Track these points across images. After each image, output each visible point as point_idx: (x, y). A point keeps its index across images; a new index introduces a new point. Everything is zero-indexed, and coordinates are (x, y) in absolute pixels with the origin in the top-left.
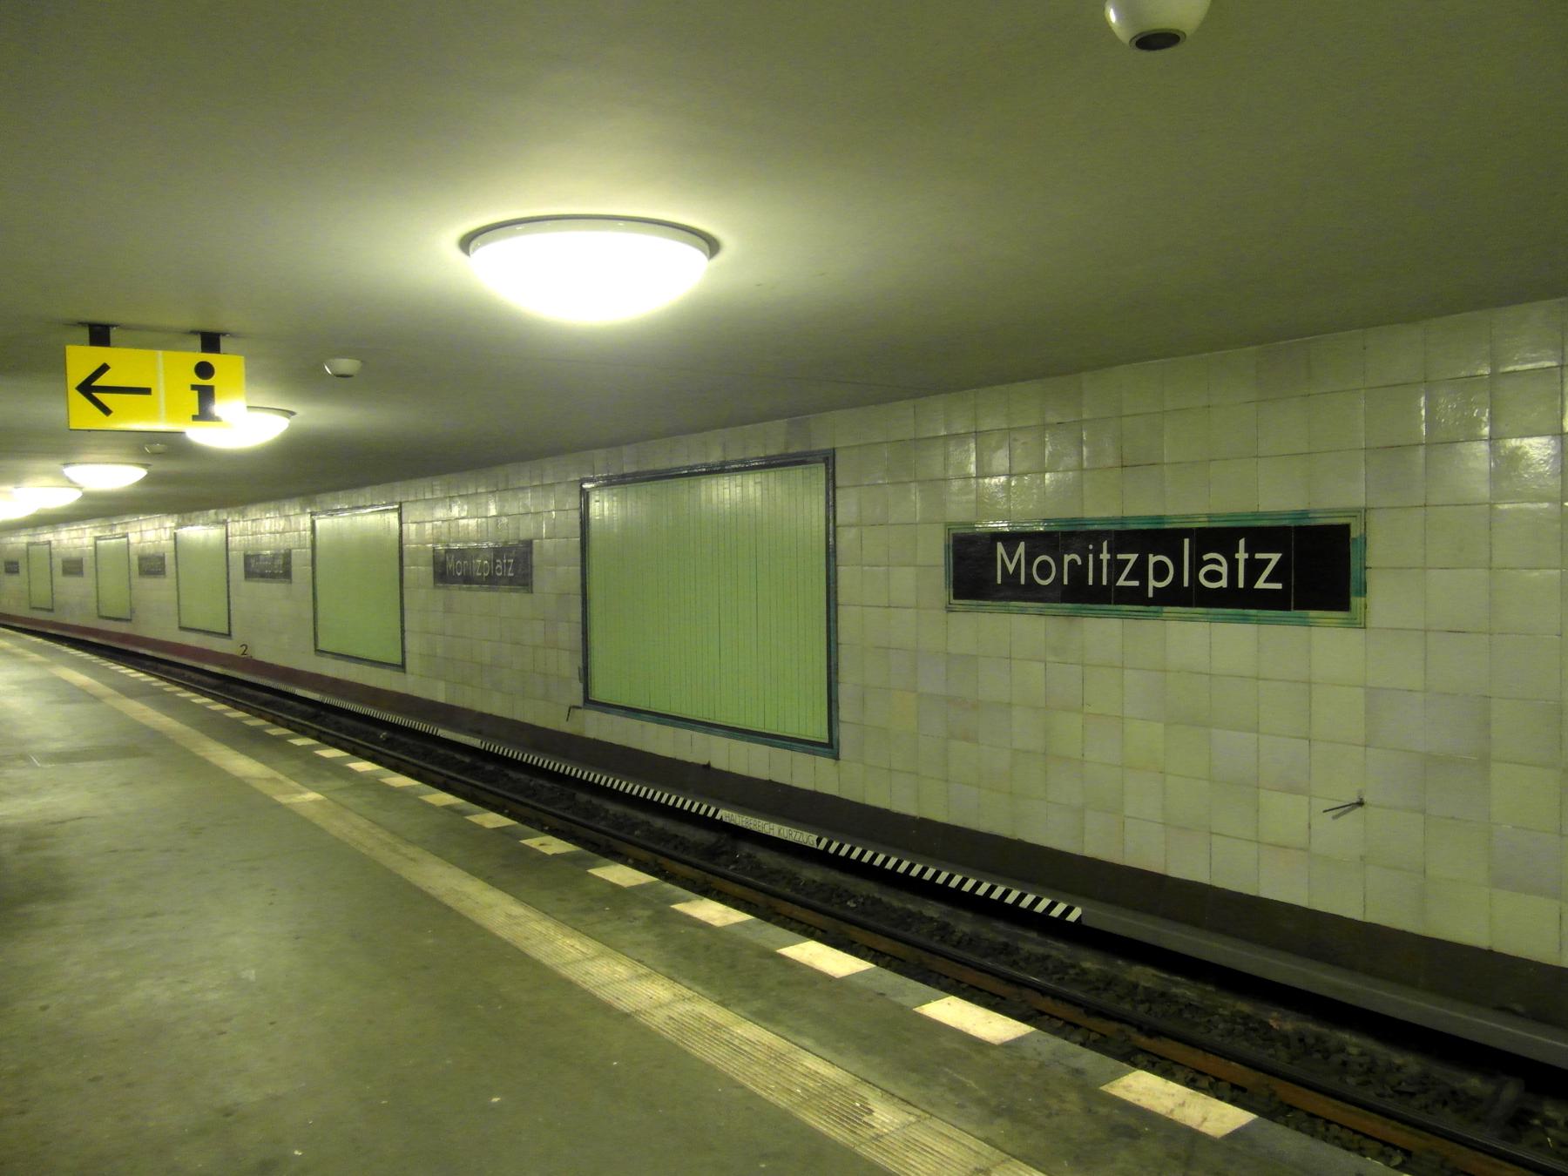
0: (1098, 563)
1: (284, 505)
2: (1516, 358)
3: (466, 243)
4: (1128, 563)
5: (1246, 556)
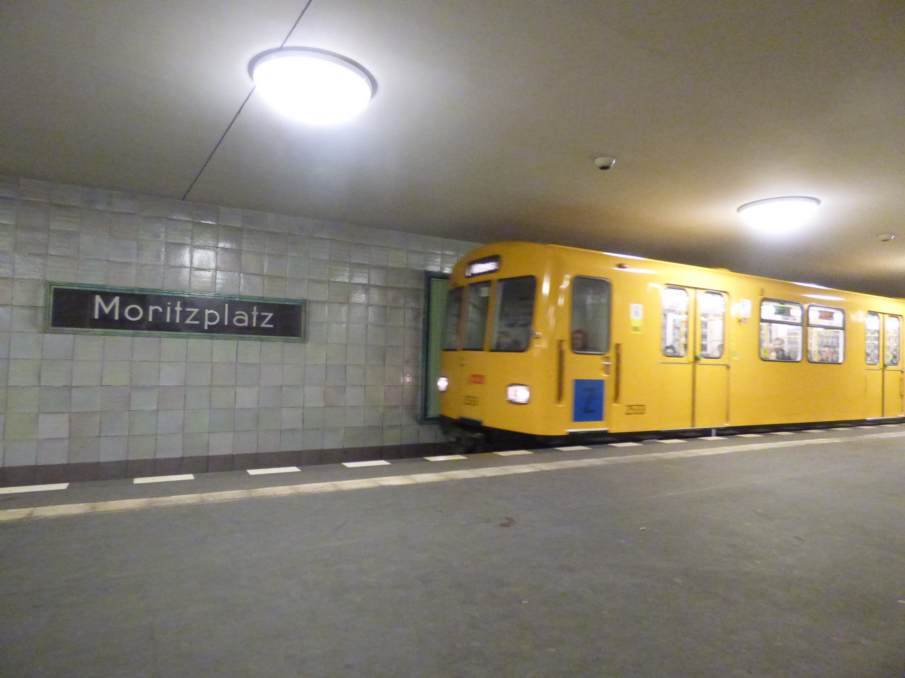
0: (173, 312)
1: (481, 291)
2: (256, 246)
3: (739, 209)
4: (191, 315)
5: (181, 309)
